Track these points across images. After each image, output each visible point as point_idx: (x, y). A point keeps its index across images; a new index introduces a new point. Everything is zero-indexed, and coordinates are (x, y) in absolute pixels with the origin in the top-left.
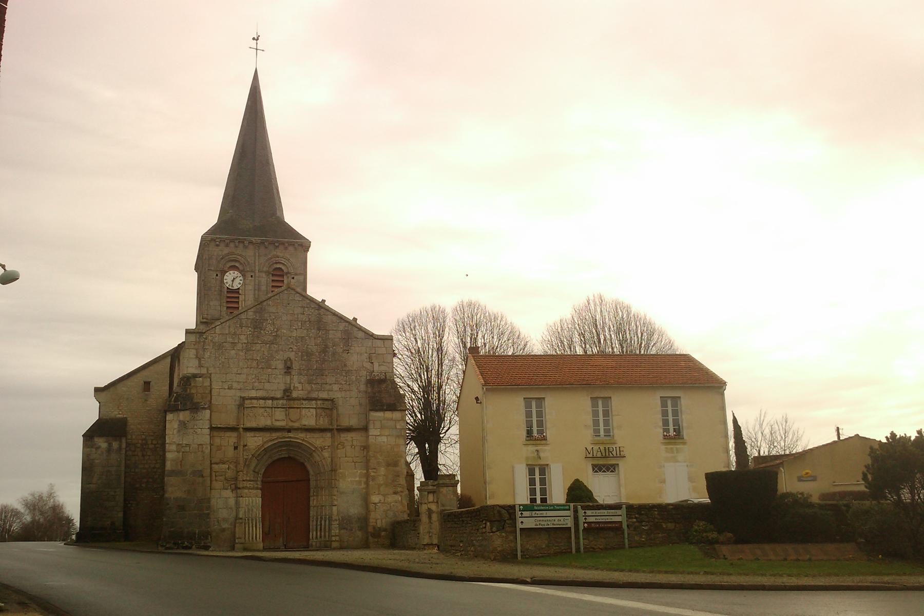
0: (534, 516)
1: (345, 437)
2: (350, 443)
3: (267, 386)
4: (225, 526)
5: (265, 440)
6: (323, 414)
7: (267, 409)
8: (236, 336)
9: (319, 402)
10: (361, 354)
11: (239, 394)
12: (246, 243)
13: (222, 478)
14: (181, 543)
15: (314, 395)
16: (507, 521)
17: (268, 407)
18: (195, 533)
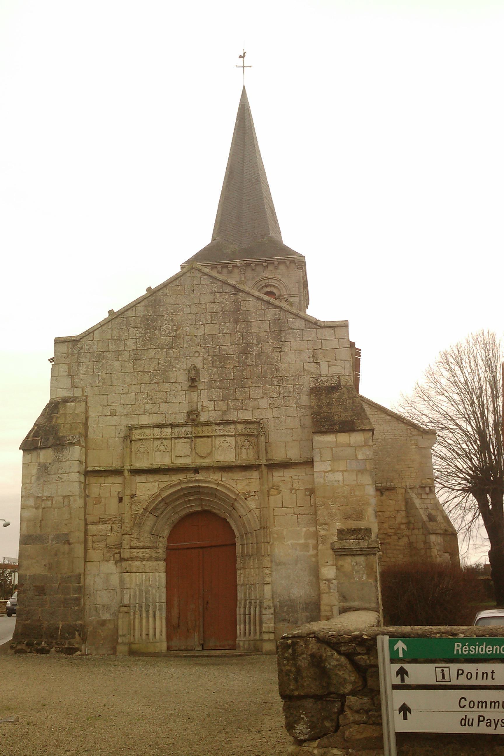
0: (454, 682)
1: (278, 475)
2: (289, 487)
3: (164, 408)
4: (106, 616)
5: (162, 486)
6: (247, 444)
7: (164, 441)
8: (121, 342)
9: (239, 427)
10: (300, 352)
11: (125, 421)
12: (230, 267)
13: (102, 545)
14: (36, 644)
15: (232, 416)
16: (352, 700)
17: (166, 438)
18: (57, 629)
